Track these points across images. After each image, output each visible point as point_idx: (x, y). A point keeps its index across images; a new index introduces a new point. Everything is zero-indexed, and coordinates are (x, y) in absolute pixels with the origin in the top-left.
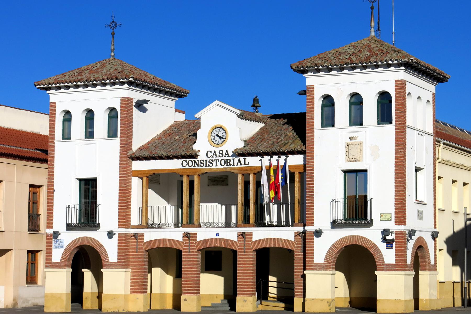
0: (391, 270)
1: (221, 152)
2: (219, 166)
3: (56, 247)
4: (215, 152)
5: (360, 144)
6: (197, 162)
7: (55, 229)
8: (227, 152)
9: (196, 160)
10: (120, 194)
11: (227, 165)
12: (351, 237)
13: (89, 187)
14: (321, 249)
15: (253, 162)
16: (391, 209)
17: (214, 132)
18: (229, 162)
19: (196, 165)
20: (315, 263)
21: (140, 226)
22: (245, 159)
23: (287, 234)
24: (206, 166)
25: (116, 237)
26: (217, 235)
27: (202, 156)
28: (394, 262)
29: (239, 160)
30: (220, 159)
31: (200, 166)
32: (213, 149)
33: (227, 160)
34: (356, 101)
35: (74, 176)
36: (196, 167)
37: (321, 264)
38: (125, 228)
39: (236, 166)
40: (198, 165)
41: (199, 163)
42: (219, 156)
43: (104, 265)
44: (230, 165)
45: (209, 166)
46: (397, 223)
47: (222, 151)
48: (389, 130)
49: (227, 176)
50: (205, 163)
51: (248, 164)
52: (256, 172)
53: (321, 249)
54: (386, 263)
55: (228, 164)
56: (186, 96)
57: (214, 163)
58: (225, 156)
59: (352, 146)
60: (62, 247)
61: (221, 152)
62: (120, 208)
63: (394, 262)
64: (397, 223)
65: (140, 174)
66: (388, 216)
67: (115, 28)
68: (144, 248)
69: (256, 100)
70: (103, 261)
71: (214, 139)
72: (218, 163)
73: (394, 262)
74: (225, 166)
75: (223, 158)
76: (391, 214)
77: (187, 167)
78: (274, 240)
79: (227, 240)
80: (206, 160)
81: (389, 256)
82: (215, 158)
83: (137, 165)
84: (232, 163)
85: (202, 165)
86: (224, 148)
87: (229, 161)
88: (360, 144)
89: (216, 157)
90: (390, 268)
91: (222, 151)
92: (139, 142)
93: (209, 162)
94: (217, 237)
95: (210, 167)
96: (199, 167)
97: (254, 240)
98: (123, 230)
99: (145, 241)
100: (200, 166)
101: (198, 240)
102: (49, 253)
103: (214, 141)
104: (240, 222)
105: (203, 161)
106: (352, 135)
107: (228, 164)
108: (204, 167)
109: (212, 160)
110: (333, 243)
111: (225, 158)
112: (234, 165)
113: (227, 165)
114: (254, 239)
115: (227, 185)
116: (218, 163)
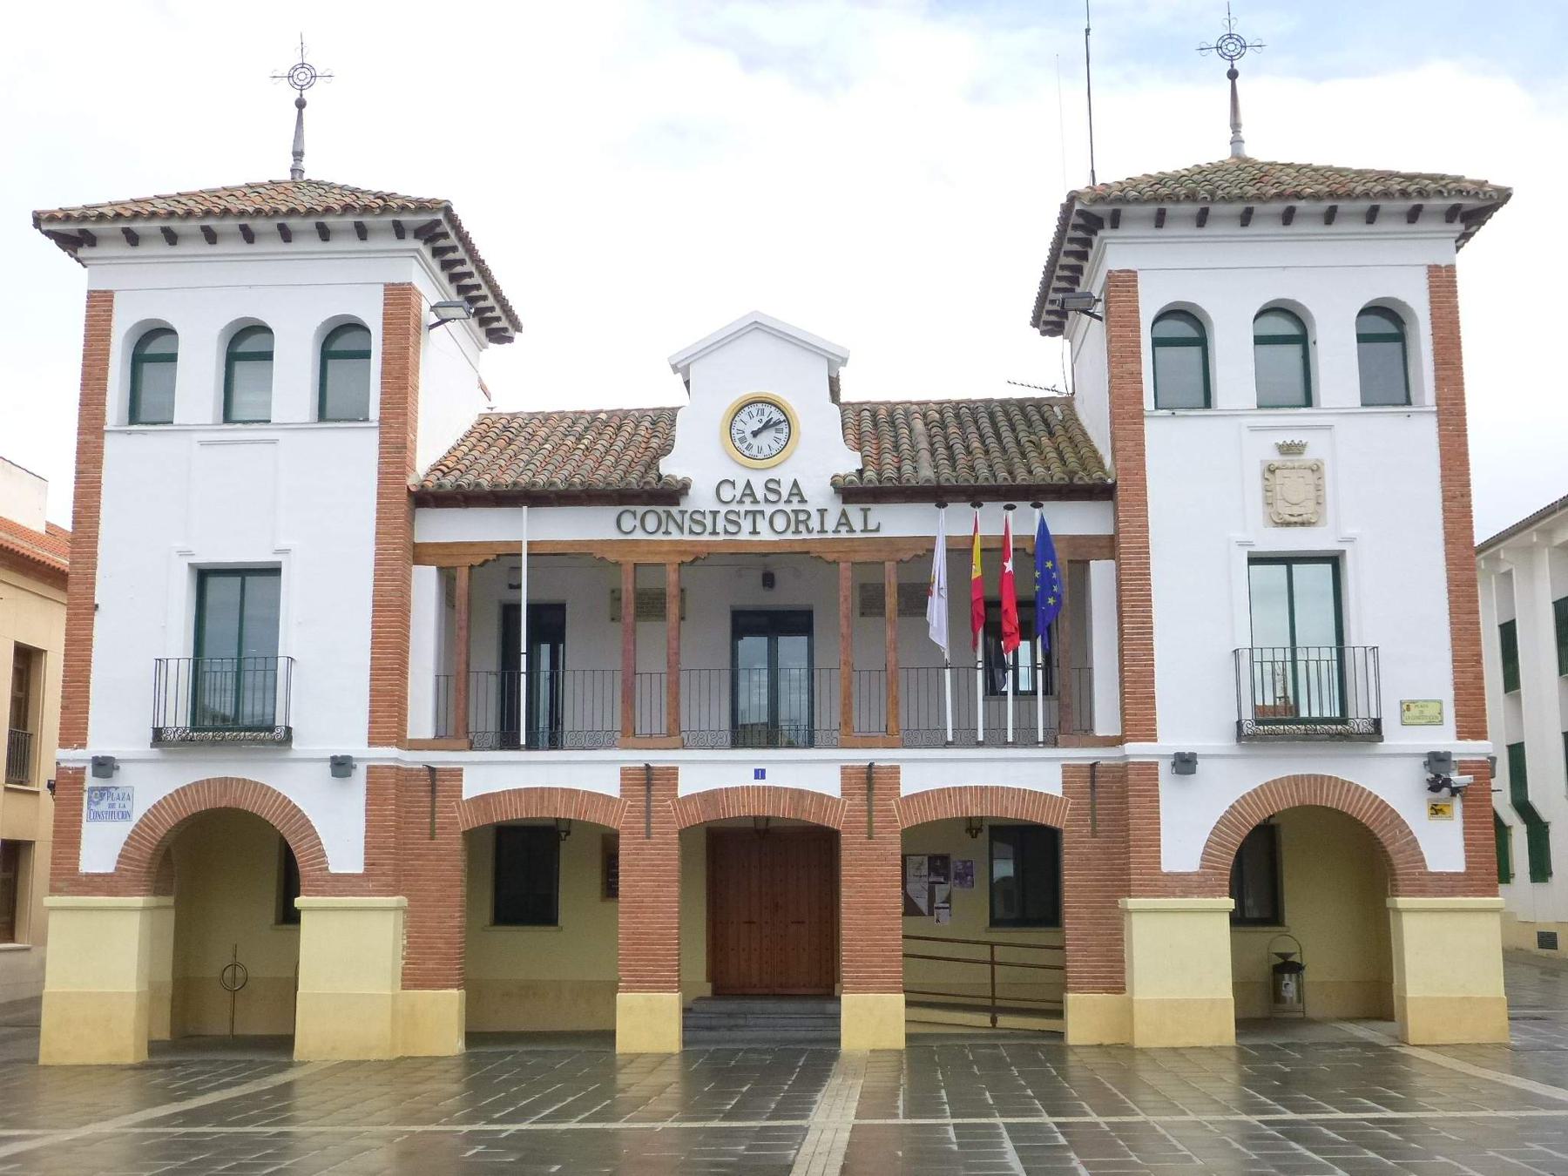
1: (772, 487)
2: (766, 535)
3: (98, 816)
4: (748, 484)
5: (1316, 469)
6: (678, 518)
7: (97, 745)
8: (795, 484)
9: (674, 510)
11: (797, 532)
12: (1297, 780)
15: (899, 522)
16: (1438, 683)
17: (744, 416)
18: (805, 522)
19: (672, 528)
20: (1167, 875)
21: (441, 741)
23: (1032, 775)
24: (714, 533)
26: (760, 774)
27: (701, 498)
28: (1460, 867)
29: (844, 514)
31: (691, 532)
32: (741, 476)
33: (796, 512)
34: (247, 345)
36: (675, 535)
37: (1189, 874)
39: (830, 535)
40: (681, 529)
42: (767, 500)
43: (304, 884)
44: (809, 531)
46: (1461, 735)
47: (778, 482)
50: (708, 521)
51: (877, 530)
52: (906, 557)
53: (1187, 829)
54: (333, 870)
55: (802, 528)
57: (747, 525)
58: (788, 501)
60: (126, 815)
62: (377, 671)
63: (1461, 868)
64: (1461, 735)
65: (447, 560)
66: (1431, 711)
67: (311, 68)
68: (469, 820)
71: (743, 440)
72: (763, 525)
73: (1461, 868)
74: (789, 536)
76: (1440, 702)
77: (639, 535)
80: (715, 513)
81: (1442, 844)
82: (748, 505)
83: (442, 527)
85: (697, 529)
86: (785, 476)
88: (1316, 469)
89: (755, 501)
90: (1446, 884)
91: (778, 482)
92: (433, 444)
93: (692, 519)
95: (728, 537)
96: (687, 537)
98: (388, 754)
100: (691, 532)
101: (681, 793)
102: (68, 837)
104: (451, 732)
105: (703, 514)
106: (1288, 437)
107: (802, 528)
108: (706, 537)
109: (738, 514)
111: (788, 509)
112: (822, 531)
113: (797, 532)
114: (468, 793)
116: (763, 525)
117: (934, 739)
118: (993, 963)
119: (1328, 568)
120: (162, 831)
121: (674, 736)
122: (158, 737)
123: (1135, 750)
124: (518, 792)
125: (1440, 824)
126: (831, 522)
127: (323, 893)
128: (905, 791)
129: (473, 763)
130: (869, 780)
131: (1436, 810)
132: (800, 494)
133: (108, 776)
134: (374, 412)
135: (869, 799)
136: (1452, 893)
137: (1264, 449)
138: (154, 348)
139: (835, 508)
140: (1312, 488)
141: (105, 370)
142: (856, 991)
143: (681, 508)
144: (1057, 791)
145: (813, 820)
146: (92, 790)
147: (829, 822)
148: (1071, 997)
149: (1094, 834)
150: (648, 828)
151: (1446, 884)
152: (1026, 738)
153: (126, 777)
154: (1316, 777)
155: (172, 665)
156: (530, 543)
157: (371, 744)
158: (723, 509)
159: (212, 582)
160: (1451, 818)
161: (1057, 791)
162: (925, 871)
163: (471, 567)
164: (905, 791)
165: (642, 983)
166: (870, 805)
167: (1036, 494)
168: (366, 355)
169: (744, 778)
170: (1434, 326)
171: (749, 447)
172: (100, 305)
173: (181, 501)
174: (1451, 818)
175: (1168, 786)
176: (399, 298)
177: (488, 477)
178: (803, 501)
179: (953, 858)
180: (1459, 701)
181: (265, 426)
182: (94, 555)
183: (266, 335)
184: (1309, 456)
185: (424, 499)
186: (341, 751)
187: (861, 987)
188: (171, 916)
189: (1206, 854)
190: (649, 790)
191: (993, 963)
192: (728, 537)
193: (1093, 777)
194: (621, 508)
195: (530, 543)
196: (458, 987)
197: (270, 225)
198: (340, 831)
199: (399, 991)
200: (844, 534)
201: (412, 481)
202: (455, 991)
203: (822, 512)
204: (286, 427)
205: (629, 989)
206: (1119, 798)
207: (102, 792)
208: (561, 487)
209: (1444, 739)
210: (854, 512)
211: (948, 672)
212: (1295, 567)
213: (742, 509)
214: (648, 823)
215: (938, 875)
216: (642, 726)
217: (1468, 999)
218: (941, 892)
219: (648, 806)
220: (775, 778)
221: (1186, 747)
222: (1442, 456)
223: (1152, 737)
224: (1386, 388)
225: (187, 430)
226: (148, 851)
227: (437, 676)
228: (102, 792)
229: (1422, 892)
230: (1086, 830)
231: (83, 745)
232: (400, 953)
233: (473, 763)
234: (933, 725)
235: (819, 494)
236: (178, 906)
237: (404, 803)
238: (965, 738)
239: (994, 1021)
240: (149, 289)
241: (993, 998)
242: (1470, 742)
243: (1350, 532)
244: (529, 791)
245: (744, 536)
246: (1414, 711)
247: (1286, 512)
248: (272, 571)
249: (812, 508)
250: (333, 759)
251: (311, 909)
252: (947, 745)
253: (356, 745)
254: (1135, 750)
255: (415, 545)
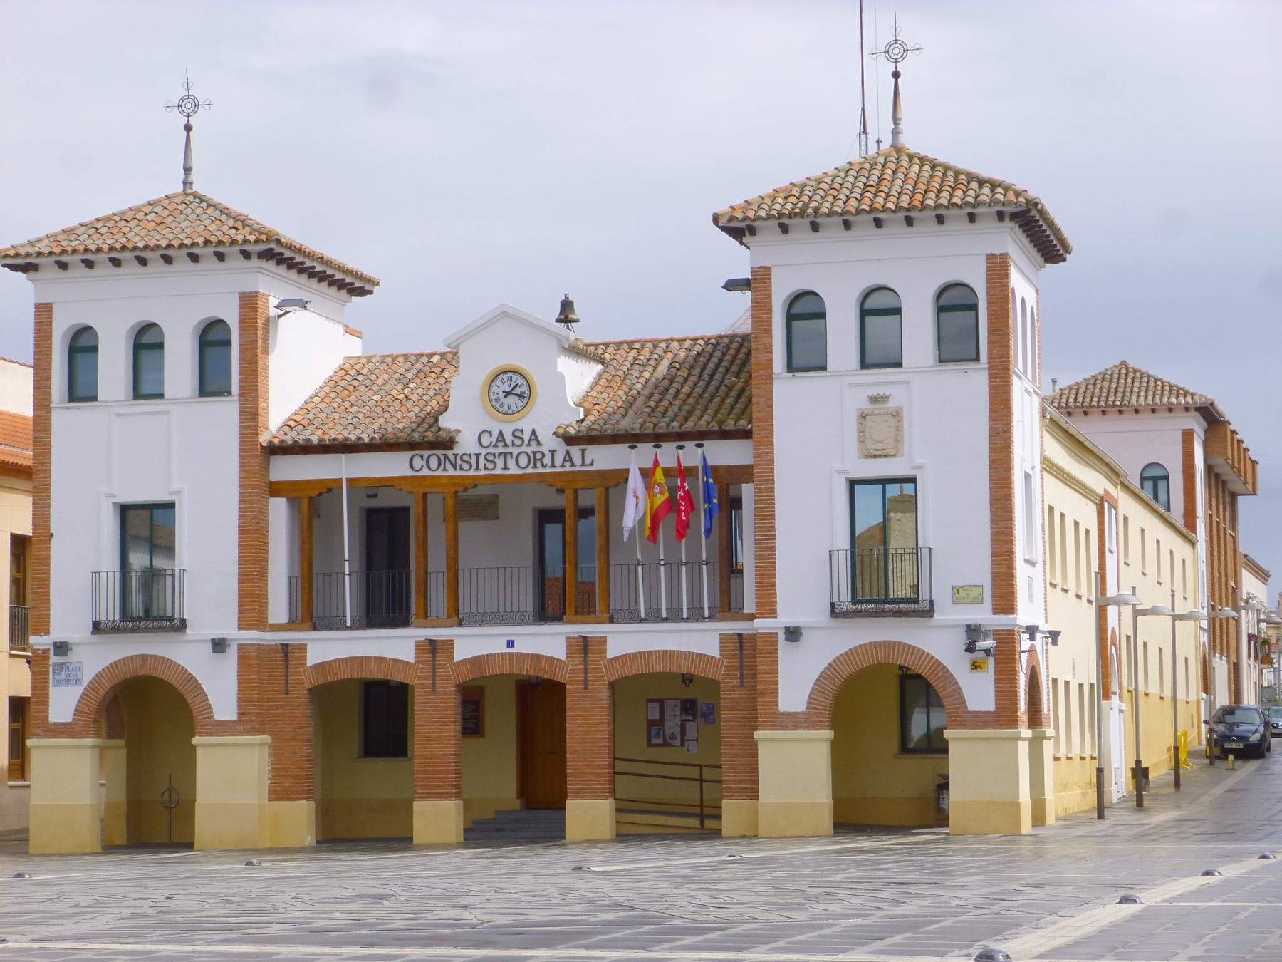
0: (985, 726)
2: (514, 470)
3: (60, 683)
4: (501, 434)
5: (897, 414)
6: (452, 458)
7: (58, 632)
8: (534, 432)
9: (450, 453)
10: (240, 544)
12: (876, 646)
13: (146, 526)
14: (796, 680)
15: (604, 458)
16: (982, 575)
17: (498, 382)
18: (541, 460)
19: (448, 466)
20: (783, 714)
21: (292, 625)
22: (583, 451)
23: (701, 640)
25: (232, 655)
26: (511, 644)
27: (467, 444)
28: (991, 707)
29: (568, 453)
30: (515, 451)
31: (461, 469)
33: (535, 453)
35: (839, 472)
36: (451, 472)
38: (258, 629)
39: (558, 470)
41: (459, 462)
42: (513, 445)
44: (544, 466)
45: (486, 468)
46: (996, 611)
48: (973, 382)
49: (497, 496)
50: (473, 461)
53: (796, 680)
54: (217, 717)
55: (539, 464)
56: (371, 292)
58: (529, 445)
59: (874, 418)
60: (78, 682)
61: (518, 434)
63: (992, 708)
64: (996, 611)
66: (975, 593)
68: (309, 681)
69: (566, 306)
70: (198, 718)
71: (497, 400)
72: (511, 463)
73: (992, 708)
75: (524, 448)
76: (982, 587)
77: (425, 472)
78: (361, 661)
79: (537, 658)
80: (478, 455)
81: (978, 692)
82: (501, 449)
84: (547, 460)
85: (466, 466)
86: (526, 425)
87: (539, 456)
89: (506, 445)
92: (282, 406)
94: (510, 650)
96: (459, 473)
97: (610, 655)
98: (252, 636)
99: (310, 663)
100: (461, 469)
103: (497, 405)
107: (539, 464)
108: (472, 473)
110: (830, 660)
111: (529, 450)
112: (553, 466)
113: (535, 467)
115: (497, 518)
116: (511, 463)
117: (632, 616)
118: (702, 780)
119: (858, 488)
120: (102, 693)
121: (456, 616)
122: (97, 627)
123: (762, 624)
124: (345, 660)
125: (978, 676)
126: (559, 459)
127: (211, 734)
128: (610, 654)
129: (314, 640)
130: (584, 646)
131: (976, 666)
132: (537, 439)
133: (65, 654)
134: (235, 389)
135: (585, 661)
136: (985, 726)
137: (858, 401)
138: (146, 339)
139: (561, 448)
140: (893, 430)
141: (49, 362)
142: (575, 798)
143: (455, 451)
144: (717, 654)
145: (546, 677)
146: (55, 664)
147: (558, 678)
148: (725, 803)
149: (742, 684)
150: (434, 684)
151: (224, 728)
152: (696, 615)
153: (73, 657)
154: (889, 643)
155: (103, 575)
156: (348, 480)
157: (240, 629)
158: (483, 452)
159: (131, 514)
160: (986, 672)
161: (717, 654)
162: (678, 712)
163: (310, 498)
164: (610, 654)
165: (430, 795)
166: (586, 665)
167: (700, 436)
168: (228, 343)
169: (500, 647)
170: (990, 303)
171: (502, 405)
172: (43, 313)
173: (107, 455)
174: (986, 672)
175: (784, 649)
176: (249, 303)
177: (319, 432)
178: (539, 444)
179: (700, 701)
180: (995, 584)
181: (159, 401)
182: (48, 497)
183: (153, 330)
184: (892, 404)
185: (275, 450)
186: (218, 633)
187: (579, 795)
188: (122, 754)
189: (811, 699)
190: (434, 657)
191: (702, 780)
192: (487, 472)
193: (741, 643)
194: (412, 453)
195: (348, 480)
196: (307, 798)
197: (102, 257)
198: (221, 691)
199: (266, 801)
200: (568, 468)
201: (264, 439)
202: (304, 802)
203: (553, 452)
204: (174, 401)
205: (421, 799)
206: (751, 657)
207: (62, 666)
208: (391, 436)
209: (983, 615)
210: (575, 451)
211: (640, 568)
212: (156, 511)
213: (497, 451)
214: (434, 680)
215: (687, 714)
216: (432, 611)
217: (993, 803)
218: (692, 729)
219: (434, 669)
220: (521, 647)
221: (792, 621)
222: (990, 403)
223: (773, 614)
224: (954, 347)
225: (108, 405)
226: (93, 705)
227: (290, 578)
228: (62, 666)
229: (774, 727)
230: (736, 682)
231: (47, 634)
232: (266, 775)
233: (314, 640)
234: (633, 606)
235: (549, 442)
236: (129, 747)
237: (266, 671)
238: (654, 616)
239: (702, 824)
240: (78, 301)
241: (702, 806)
242: (1002, 616)
243: (919, 460)
244: (352, 659)
245: (499, 471)
246: (962, 594)
247: (872, 447)
248: (170, 506)
249: (545, 449)
250: (213, 640)
251: (766, 740)
252: (641, 621)
253: (228, 628)
254: (762, 624)
255: (271, 483)
